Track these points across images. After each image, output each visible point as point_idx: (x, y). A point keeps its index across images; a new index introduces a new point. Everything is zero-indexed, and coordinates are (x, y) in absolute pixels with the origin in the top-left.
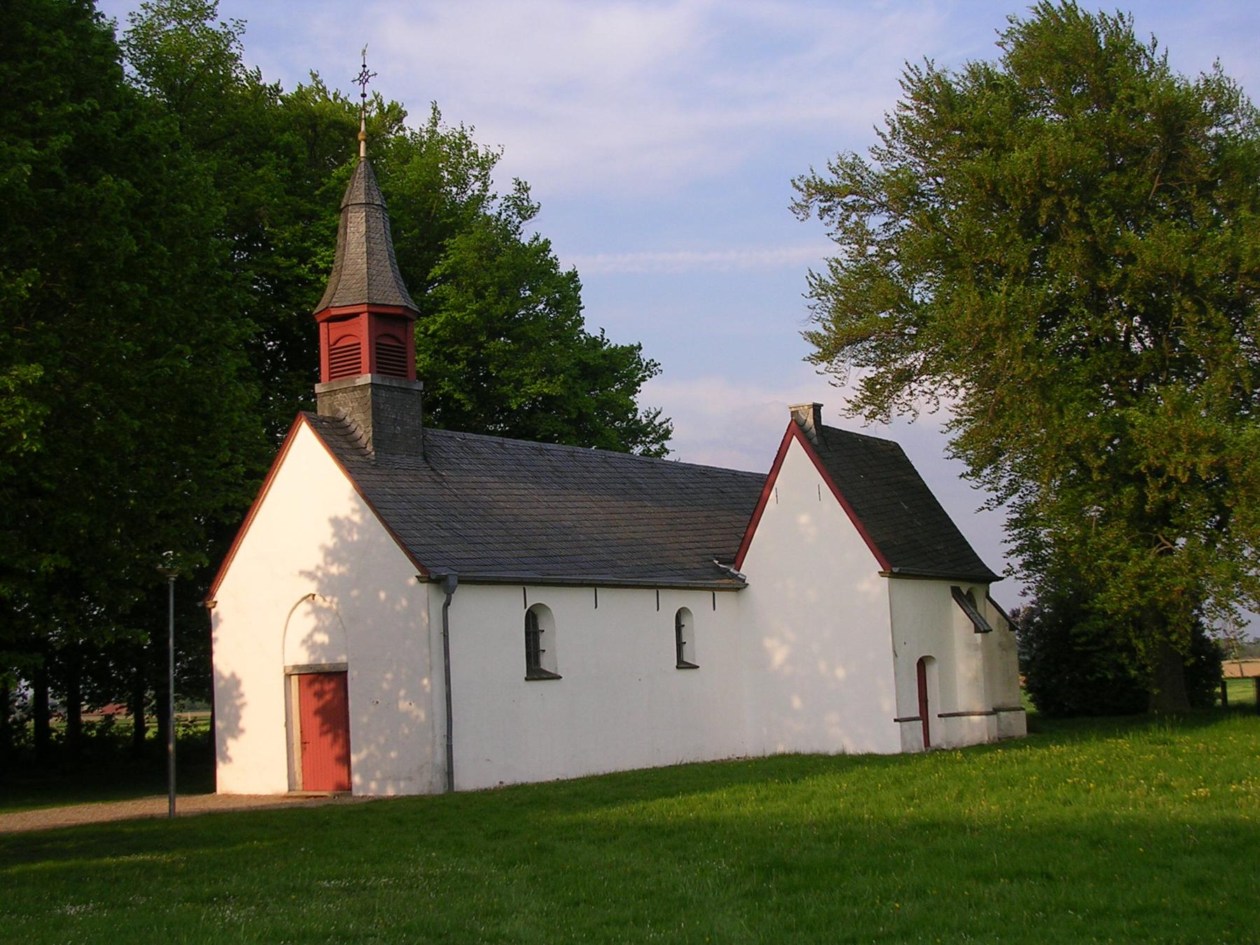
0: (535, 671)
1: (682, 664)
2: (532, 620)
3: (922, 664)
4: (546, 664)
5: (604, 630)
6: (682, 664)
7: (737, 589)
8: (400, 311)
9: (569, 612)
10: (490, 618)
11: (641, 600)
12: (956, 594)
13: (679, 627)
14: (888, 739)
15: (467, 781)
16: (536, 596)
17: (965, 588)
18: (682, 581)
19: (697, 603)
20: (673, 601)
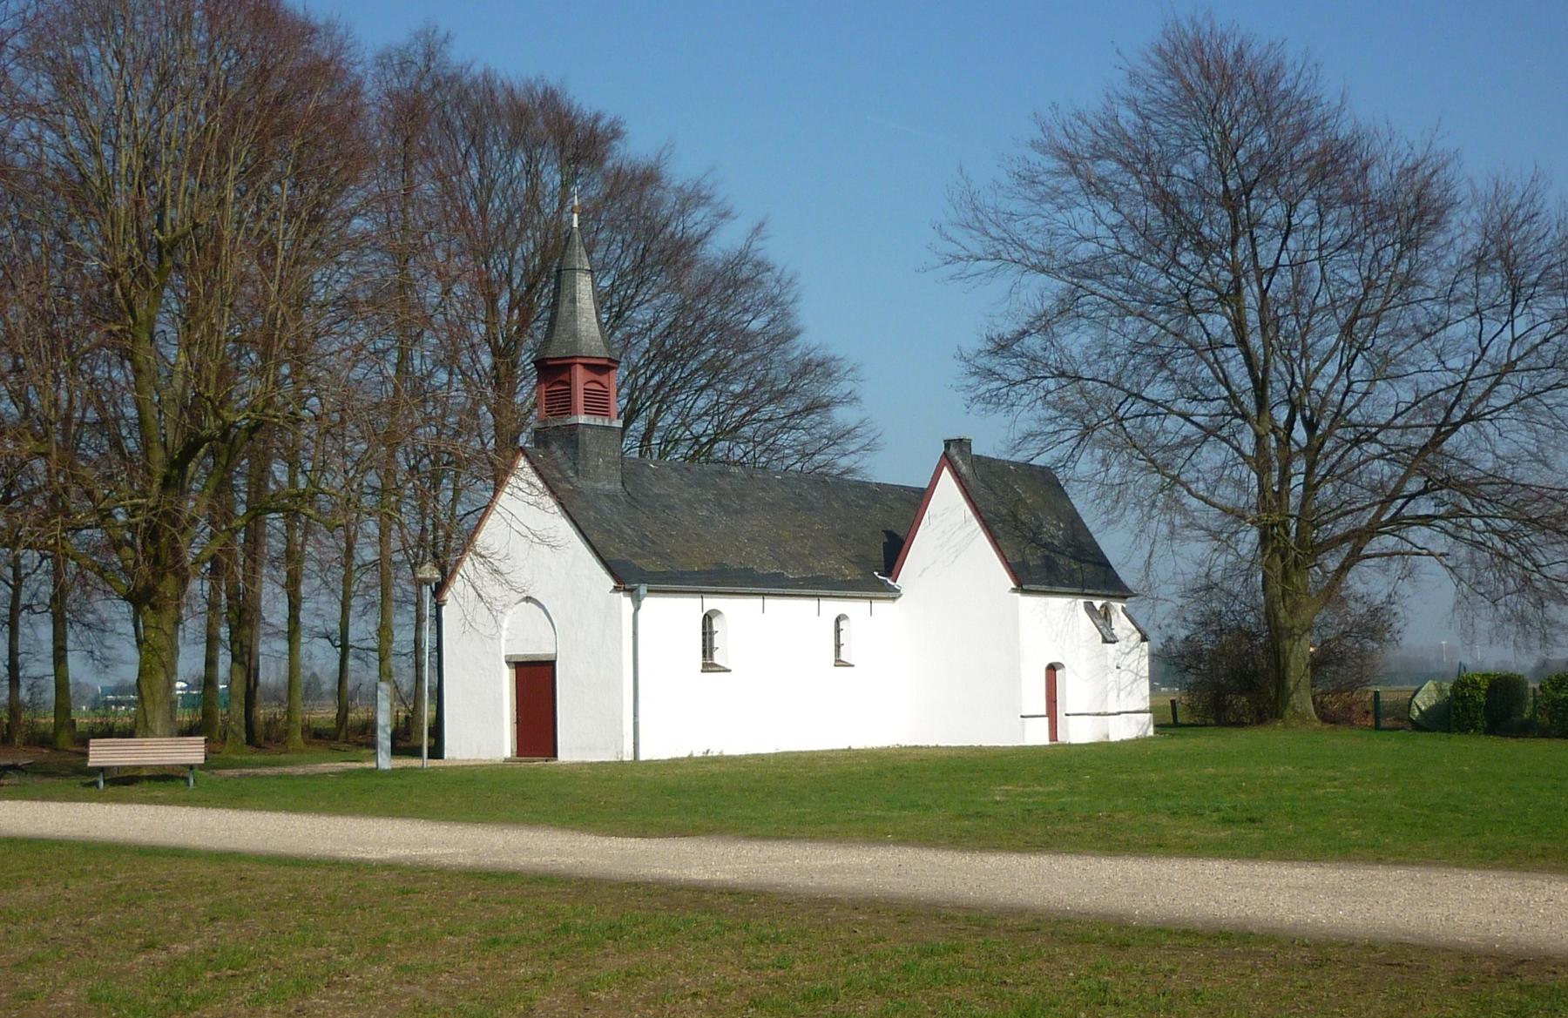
0: (709, 666)
1: (839, 663)
2: (708, 619)
3: (1052, 669)
4: (718, 658)
5: (774, 631)
6: (839, 663)
7: (894, 599)
8: (605, 362)
9: (741, 615)
10: (671, 617)
11: (808, 605)
12: (1090, 608)
13: (838, 631)
14: (1047, 742)
15: (643, 757)
16: (712, 603)
17: (1098, 603)
18: (1043, 588)
19: (854, 608)
20: (832, 607)
